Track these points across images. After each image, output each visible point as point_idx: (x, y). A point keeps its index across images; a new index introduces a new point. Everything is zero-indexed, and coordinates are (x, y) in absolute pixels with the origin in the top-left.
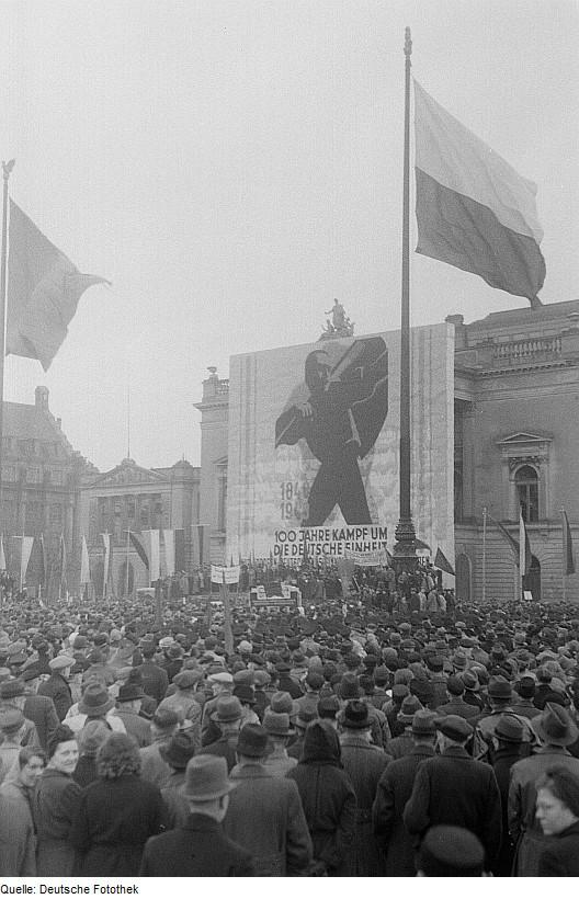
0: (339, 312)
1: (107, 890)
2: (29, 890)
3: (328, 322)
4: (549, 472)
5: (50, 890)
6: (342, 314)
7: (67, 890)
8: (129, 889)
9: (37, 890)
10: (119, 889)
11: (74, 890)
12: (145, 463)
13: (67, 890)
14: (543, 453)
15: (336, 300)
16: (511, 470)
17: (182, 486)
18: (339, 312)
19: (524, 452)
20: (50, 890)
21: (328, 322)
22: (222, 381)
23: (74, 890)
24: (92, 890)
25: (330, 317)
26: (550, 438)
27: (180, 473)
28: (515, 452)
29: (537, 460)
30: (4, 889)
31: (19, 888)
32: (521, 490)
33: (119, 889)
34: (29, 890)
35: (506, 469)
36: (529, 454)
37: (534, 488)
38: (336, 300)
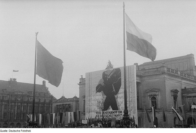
1: (24, 131)
2: (6, 131)
3: (107, 65)
5: (11, 131)
7: (15, 131)
8: (29, 131)
9: (8, 131)
10: (27, 131)
11: (17, 131)
12: (67, 97)
13: (15, 131)
15: (109, 60)
16: (150, 98)
19: (153, 93)
21: (107, 65)
23: (17, 131)
24: (21, 131)
25: (108, 64)
28: (151, 94)
29: (156, 95)
30: (1, 131)
31: (4, 131)
33: (27, 131)
34: (6, 131)
36: (152, 94)
37: (155, 102)
38: (109, 60)
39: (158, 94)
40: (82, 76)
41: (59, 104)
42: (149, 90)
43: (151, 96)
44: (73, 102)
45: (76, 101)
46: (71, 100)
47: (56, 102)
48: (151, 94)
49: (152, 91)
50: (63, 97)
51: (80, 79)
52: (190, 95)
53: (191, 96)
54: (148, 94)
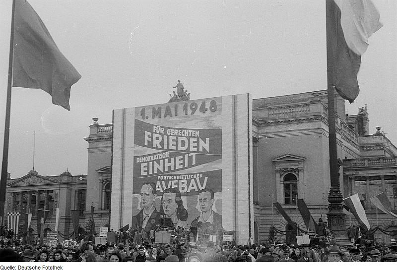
0: (180, 87)
1: (49, 268)
2: (13, 268)
3: (174, 92)
4: (302, 178)
5: (23, 268)
6: (182, 88)
7: (30, 268)
8: (59, 267)
9: (17, 268)
10: (54, 267)
11: (34, 268)
12: (43, 172)
13: (30, 268)
14: (301, 166)
15: (179, 81)
16: (281, 176)
17: (66, 186)
18: (180, 87)
19: (289, 166)
20: (23, 268)
21: (174, 92)
22: (101, 126)
23: (34, 268)
24: (42, 267)
25: (176, 90)
26: (303, 160)
27: (65, 179)
28: (283, 166)
29: (297, 170)
30: (2, 267)
31: (8, 267)
32: (286, 187)
33: (54, 267)
34: (13, 268)
35: (278, 175)
36: (292, 167)
37: (295, 186)
38: (179, 81)
39: (302, 166)
40: (95, 119)
41: (20, 190)
42: (277, 157)
43: (106, 182)
44: (60, 184)
45: (68, 184)
46: (54, 181)
47: (11, 186)
48: (104, 178)
49: (290, 158)
50: (33, 174)
51: (91, 127)
52: (362, 173)
53: (366, 175)
54: (278, 168)
